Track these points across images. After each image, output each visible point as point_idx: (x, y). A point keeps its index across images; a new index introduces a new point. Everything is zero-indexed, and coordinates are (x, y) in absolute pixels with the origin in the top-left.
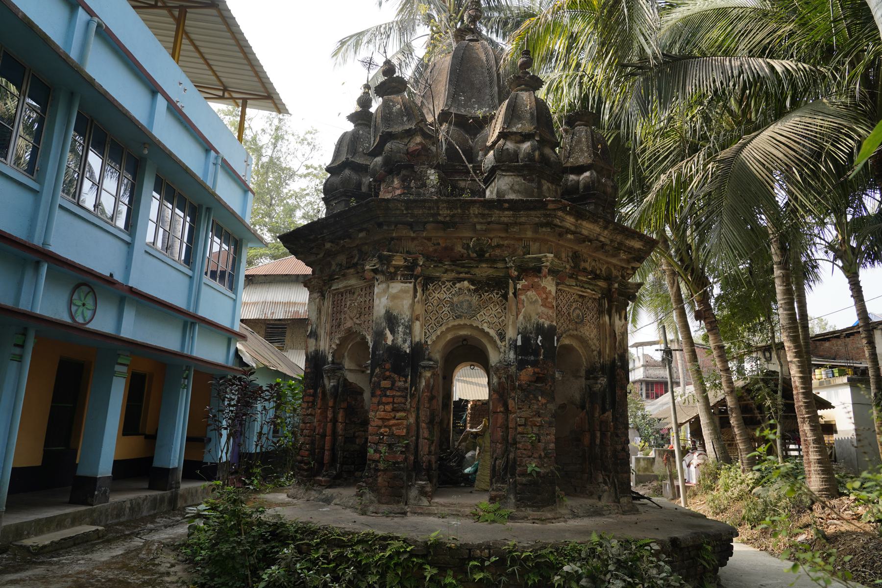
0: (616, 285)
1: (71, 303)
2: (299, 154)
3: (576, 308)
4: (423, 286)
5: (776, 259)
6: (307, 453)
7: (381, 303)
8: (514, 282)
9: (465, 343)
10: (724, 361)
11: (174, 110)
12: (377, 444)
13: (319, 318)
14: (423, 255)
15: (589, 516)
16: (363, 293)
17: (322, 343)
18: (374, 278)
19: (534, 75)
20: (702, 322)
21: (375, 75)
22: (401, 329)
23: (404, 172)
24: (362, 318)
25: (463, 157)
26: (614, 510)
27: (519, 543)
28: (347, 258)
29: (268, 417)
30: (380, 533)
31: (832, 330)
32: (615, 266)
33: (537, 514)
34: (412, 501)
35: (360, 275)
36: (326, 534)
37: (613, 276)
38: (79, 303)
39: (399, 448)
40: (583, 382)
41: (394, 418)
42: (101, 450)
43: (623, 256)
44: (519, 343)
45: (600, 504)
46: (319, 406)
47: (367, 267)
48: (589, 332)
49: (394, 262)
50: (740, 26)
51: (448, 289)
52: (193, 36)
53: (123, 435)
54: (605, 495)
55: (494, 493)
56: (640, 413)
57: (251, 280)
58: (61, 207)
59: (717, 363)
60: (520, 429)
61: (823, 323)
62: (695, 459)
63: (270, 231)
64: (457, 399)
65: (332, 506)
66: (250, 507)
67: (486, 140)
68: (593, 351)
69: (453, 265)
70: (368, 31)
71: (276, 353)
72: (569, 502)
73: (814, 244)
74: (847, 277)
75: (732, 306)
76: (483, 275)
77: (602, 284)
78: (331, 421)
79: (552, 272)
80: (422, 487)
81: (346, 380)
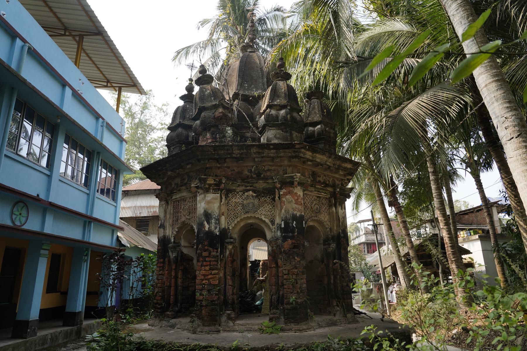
0: (338, 190)
1: (12, 213)
2: (157, 117)
3: (315, 204)
4: (226, 195)
5: (430, 170)
6: (160, 298)
7: (201, 207)
8: (278, 190)
9: (252, 227)
10: (407, 229)
11: (76, 95)
12: (201, 290)
13: (165, 216)
14: (225, 177)
15: (328, 326)
16: (191, 200)
17: (167, 231)
18: (197, 191)
19: (286, 72)
20: (393, 207)
21: (195, 74)
22: (213, 221)
23: (212, 129)
24: (191, 215)
25: (248, 119)
26: (343, 322)
27: (286, 345)
28: (181, 180)
29: (137, 277)
30: (203, 344)
31: (471, 208)
32: (337, 179)
33: (297, 327)
34: (223, 324)
35: (189, 189)
36: (170, 347)
37: (337, 184)
38: (18, 213)
39: (214, 292)
40: (322, 246)
41: (211, 274)
42: (31, 303)
43: (341, 173)
44: (283, 226)
45: (335, 319)
46: (166, 269)
47: (193, 185)
48: (324, 217)
49: (208, 182)
50: (401, 41)
51: (241, 196)
52: (88, 52)
53: (47, 293)
54: (338, 313)
55: (271, 316)
56: (363, 262)
57: (126, 194)
58: (6, 156)
59: (403, 231)
60: (285, 277)
61: (466, 204)
62: (395, 288)
63: (139, 163)
64: (254, 260)
65: (176, 330)
66: (124, 334)
67: (260, 109)
68: (327, 228)
69: (243, 182)
70: (193, 45)
71: (143, 237)
72: (317, 318)
73: (454, 159)
74: (474, 178)
75: (410, 197)
76: (261, 187)
77: (330, 189)
78: (174, 278)
79: (300, 184)
80: (229, 315)
81: (182, 252)
